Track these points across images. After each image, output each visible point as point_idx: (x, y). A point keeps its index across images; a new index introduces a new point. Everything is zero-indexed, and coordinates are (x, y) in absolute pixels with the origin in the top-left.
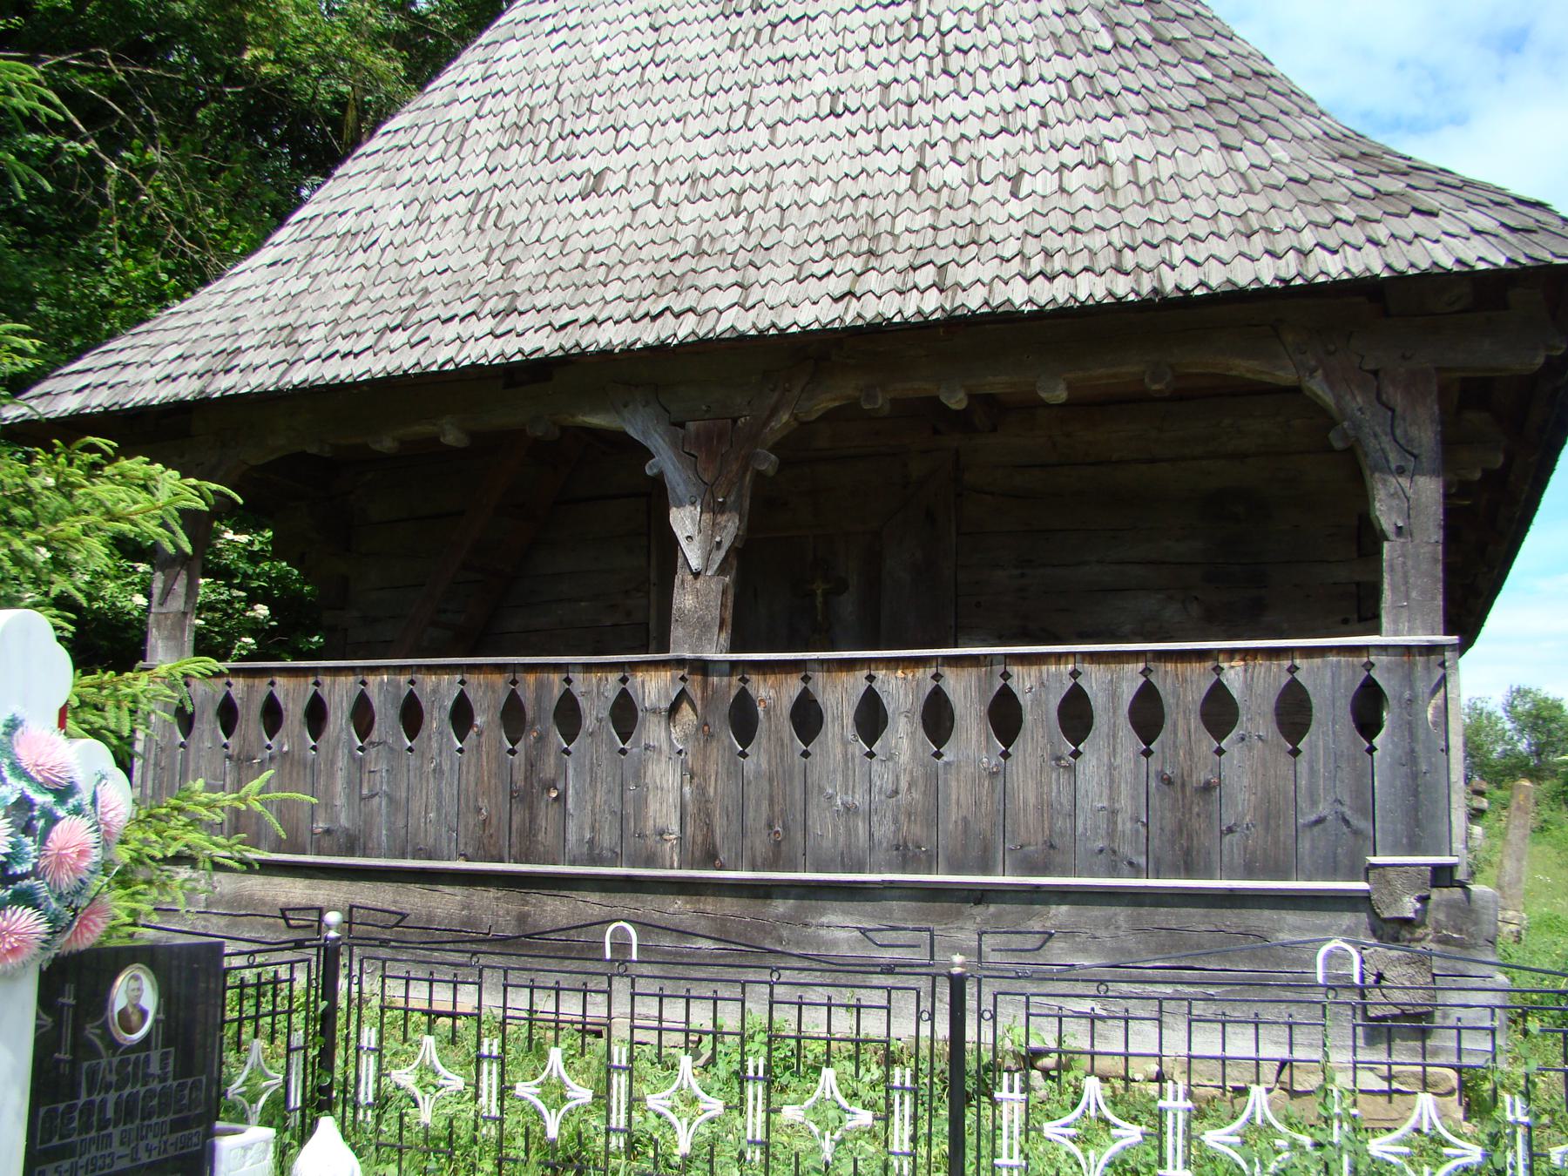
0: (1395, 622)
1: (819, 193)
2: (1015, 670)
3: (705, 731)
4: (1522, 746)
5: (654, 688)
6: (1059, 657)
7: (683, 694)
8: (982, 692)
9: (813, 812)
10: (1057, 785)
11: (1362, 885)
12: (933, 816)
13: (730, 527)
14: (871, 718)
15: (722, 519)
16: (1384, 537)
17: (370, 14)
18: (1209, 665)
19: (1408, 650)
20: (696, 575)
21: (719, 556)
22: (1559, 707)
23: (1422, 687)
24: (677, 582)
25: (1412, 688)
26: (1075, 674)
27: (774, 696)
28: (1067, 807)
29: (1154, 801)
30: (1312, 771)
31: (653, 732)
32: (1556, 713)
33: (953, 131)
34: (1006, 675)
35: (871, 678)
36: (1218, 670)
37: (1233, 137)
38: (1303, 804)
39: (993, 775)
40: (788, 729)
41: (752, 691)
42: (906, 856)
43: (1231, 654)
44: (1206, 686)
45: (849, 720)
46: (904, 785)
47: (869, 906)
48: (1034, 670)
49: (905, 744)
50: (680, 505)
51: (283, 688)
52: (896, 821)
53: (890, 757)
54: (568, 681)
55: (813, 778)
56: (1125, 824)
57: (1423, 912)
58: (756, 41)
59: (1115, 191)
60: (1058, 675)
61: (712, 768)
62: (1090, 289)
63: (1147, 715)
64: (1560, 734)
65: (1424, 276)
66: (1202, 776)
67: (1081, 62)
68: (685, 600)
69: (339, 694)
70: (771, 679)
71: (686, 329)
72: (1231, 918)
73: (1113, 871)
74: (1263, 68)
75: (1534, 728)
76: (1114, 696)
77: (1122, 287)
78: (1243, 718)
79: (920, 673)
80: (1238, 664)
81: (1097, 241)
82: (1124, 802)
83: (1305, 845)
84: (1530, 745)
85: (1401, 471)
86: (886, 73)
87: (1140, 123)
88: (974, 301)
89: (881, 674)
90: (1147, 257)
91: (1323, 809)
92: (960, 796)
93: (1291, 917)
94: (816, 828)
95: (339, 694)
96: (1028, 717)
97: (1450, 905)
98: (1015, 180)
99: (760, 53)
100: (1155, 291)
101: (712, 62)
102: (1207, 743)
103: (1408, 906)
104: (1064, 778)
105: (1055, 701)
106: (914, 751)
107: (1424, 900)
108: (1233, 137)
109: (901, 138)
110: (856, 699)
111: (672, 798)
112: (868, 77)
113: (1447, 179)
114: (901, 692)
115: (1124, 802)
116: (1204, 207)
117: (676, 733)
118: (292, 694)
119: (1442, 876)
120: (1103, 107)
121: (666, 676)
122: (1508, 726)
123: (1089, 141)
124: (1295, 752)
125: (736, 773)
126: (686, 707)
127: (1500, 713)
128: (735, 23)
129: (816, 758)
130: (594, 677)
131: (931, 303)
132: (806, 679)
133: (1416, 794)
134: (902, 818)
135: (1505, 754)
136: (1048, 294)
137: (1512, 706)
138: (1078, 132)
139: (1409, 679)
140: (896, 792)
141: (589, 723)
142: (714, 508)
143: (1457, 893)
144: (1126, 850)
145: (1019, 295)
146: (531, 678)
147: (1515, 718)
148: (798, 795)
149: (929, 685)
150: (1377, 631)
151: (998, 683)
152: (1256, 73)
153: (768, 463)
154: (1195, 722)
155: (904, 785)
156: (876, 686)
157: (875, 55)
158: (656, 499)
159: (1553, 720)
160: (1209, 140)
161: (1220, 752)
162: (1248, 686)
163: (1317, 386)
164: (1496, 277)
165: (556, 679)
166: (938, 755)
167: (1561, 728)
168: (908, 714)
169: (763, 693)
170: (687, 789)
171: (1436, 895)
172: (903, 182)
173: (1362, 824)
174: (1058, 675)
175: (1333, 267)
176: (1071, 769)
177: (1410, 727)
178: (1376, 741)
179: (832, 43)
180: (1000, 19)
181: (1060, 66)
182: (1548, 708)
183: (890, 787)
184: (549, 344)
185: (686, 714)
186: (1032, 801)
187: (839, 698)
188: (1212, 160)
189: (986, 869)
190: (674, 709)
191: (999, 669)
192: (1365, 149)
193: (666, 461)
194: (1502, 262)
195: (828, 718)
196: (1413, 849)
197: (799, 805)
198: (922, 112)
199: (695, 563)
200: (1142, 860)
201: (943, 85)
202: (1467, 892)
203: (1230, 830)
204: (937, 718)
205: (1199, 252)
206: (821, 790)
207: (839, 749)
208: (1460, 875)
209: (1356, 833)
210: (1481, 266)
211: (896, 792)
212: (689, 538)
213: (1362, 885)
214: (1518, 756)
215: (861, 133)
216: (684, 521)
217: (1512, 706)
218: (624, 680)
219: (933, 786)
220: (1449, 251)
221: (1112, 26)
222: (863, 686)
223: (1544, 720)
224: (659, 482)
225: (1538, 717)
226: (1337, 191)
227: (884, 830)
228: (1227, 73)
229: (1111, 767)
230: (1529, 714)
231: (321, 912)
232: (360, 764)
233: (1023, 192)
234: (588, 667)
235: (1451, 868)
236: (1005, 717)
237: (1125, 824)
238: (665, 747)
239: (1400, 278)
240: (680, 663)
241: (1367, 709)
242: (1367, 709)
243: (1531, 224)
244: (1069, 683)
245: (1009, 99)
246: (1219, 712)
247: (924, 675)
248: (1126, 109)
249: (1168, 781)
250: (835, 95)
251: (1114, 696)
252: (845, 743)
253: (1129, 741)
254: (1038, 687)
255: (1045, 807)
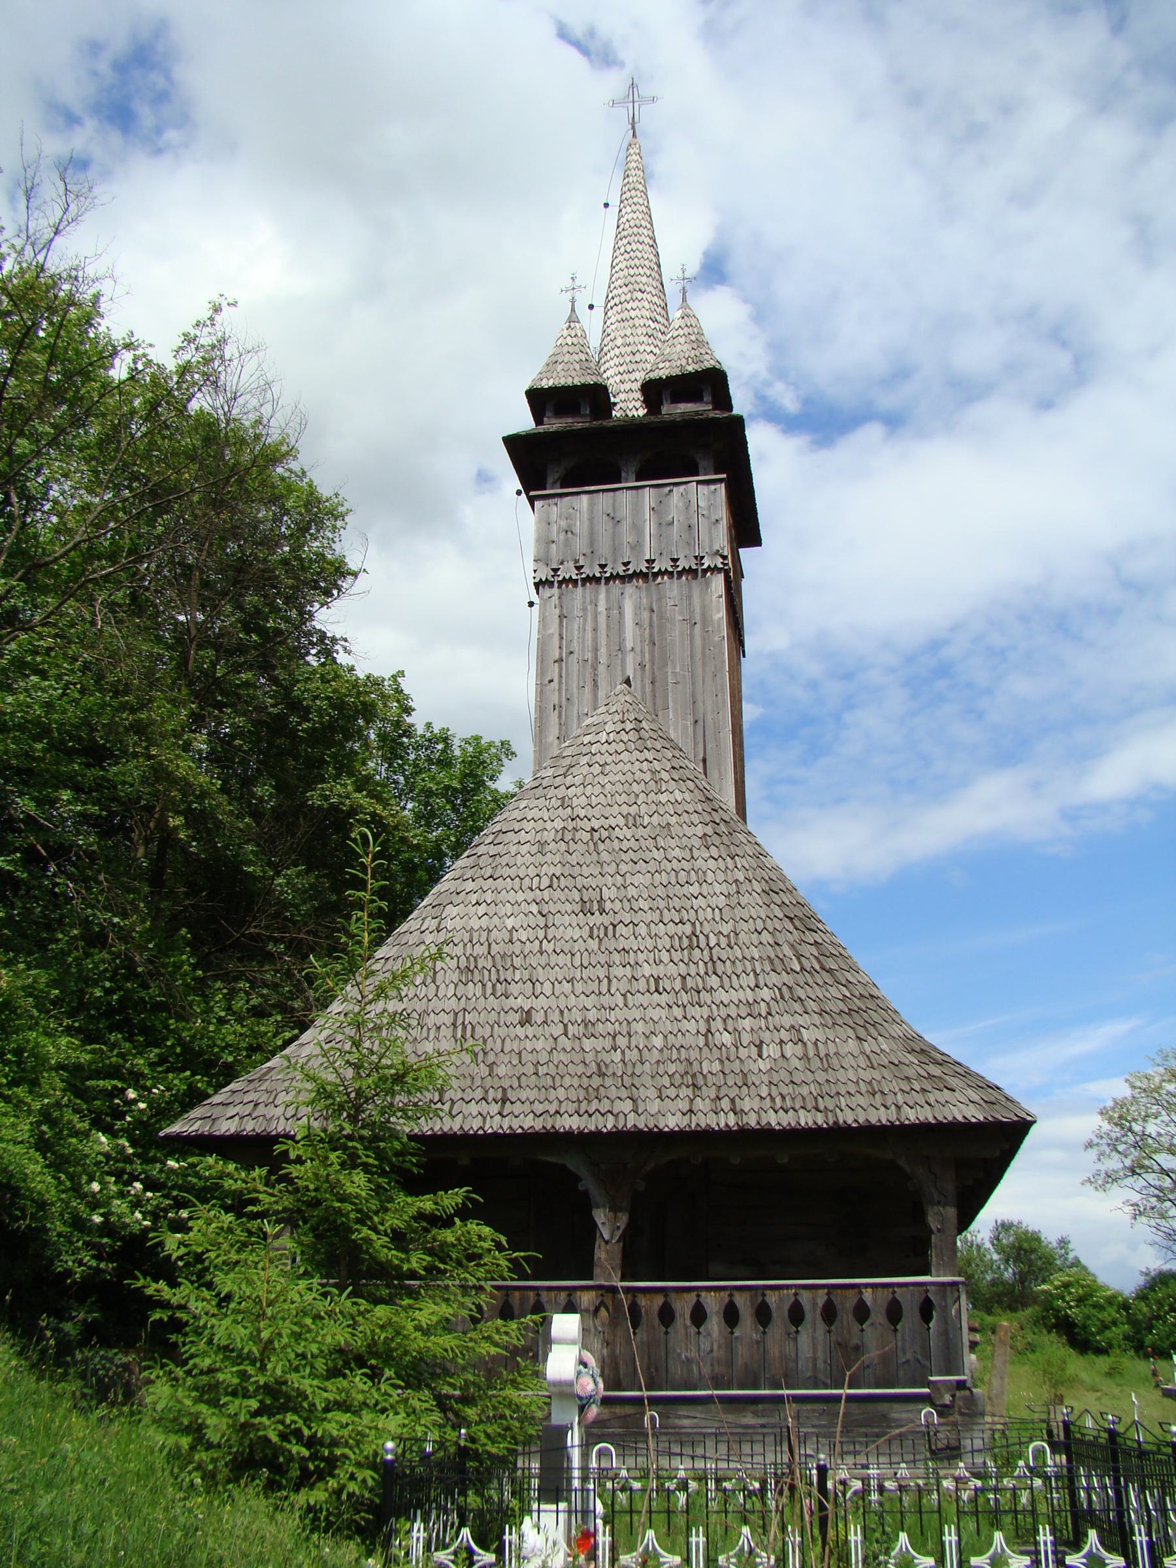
0: (938, 1271)
1: (658, 1041)
2: (768, 1292)
3: (614, 1322)
4: (1008, 1274)
6: (788, 1287)
7: (602, 1303)
8: (752, 1304)
9: (671, 1362)
10: (789, 1348)
11: (927, 1390)
12: (730, 1362)
13: (623, 1220)
14: (699, 1315)
15: (620, 1215)
16: (932, 1232)
18: (856, 1290)
19: (943, 1284)
20: (607, 1242)
21: (618, 1233)
22: (1038, 1240)
23: (949, 1301)
24: (597, 1246)
25: (946, 1301)
26: (796, 1294)
28: (793, 1355)
29: (834, 1354)
30: (903, 1339)
32: (1035, 1245)
33: (723, 1012)
34: (764, 1295)
35: (698, 1296)
36: (861, 1293)
37: (862, 1033)
38: (900, 1354)
39: (758, 1342)
40: (656, 1321)
41: (639, 1302)
42: (717, 1383)
43: (866, 1285)
44: (855, 1300)
45: (688, 1316)
46: (715, 1347)
47: (700, 1408)
48: (777, 1293)
49: (716, 1328)
50: (598, 1207)
52: (712, 1365)
53: (709, 1334)
54: (538, 1295)
55: (670, 1345)
56: (820, 1365)
57: (953, 1402)
58: (606, 935)
59: (809, 1059)
60: (788, 1295)
61: (618, 1340)
62: (806, 1119)
63: (829, 1313)
64: (1039, 1263)
65: (950, 1124)
66: (855, 1341)
67: (785, 978)
68: (600, 1254)
70: (648, 1296)
71: (609, 1124)
72: (870, 1407)
73: (816, 1387)
74: (875, 992)
75: (1017, 1259)
76: (815, 1304)
77: (820, 1119)
78: (872, 1315)
79: (722, 1293)
80: (869, 1290)
81: (805, 1090)
82: (820, 1354)
83: (901, 1373)
84: (1014, 1274)
85: (939, 1203)
86: (683, 969)
87: (817, 1019)
88: (752, 1121)
89: (703, 1294)
90: (829, 1103)
91: (909, 1356)
92: (743, 1353)
93: (897, 1406)
94: (672, 1369)
96: (774, 1315)
97: (964, 1398)
98: (759, 1047)
99: (610, 944)
100: (835, 1123)
101: (580, 945)
102: (856, 1327)
103: (947, 1399)
104: (792, 1343)
105: (786, 1307)
106: (720, 1331)
107: (953, 1396)
108: (862, 1033)
109: (696, 1011)
110: (691, 1306)
112: (672, 970)
113: (959, 1070)
114: (713, 1304)
115: (820, 1354)
116: (851, 1075)
117: (598, 1322)
119: (961, 1385)
120: (797, 1007)
122: (995, 1257)
123: (793, 1027)
124: (896, 1330)
126: (603, 1310)
127: (988, 1245)
128: (591, 920)
129: (672, 1336)
130: (553, 1294)
131: (732, 1120)
132: (666, 1296)
133: (948, 1348)
134: (715, 1363)
135: (993, 1283)
136: (786, 1120)
137: (997, 1238)
138: (787, 1020)
139: (944, 1298)
140: (712, 1351)
142: (615, 1209)
143: (967, 1393)
144: (822, 1377)
145: (774, 1120)
146: (517, 1294)
147: (1000, 1249)
148: (663, 1353)
149: (727, 1300)
150: (926, 1271)
151: (760, 1299)
152: (872, 996)
153: (641, 1186)
154: (851, 1316)
155: (715, 1347)
156: (701, 1300)
157: (677, 956)
158: (585, 1207)
159: (1033, 1251)
160: (851, 1033)
161: (862, 1330)
162: (874, 1300)
163: (902, 1163)
164: (979, 1125)
165: (532, 1294)
166: (732, 1333)
167: (1040, 1258)
168: (717, 1313)
169: (643, 1303)
170: (605, 1351)
171: (958, 1394)
172: (701, 1041)
173: (927, 1363)
174: (788, 1295)
175: (911, 1116)
176: (795, 1339)
177: (945, 1319)
178: (931, 1325)
179: (649, 943)
180: (740, 943)
181: (773, 978)
182: (1026, 1240)
183: (708, 1349)
184: (529, 1123)
185: (603, 1312)
186: (777, 1354)
187: (683, 1307)
188: (852, 1045)
189: (756, 1387)
190: (597, 1310)
191: (760, 1292)
192: (924, 1048)
193: (588, 1184)
194: (982, 1119)
195: (677, 1315)
196: (948, 1373)
197: (664, 1358)
198: (705, 997)
199: (606, 1236)
200: (829, 1382)
201: (714, 981)
202: (971, 1392)
203: (868, 1366)
204: (731, 1316)
205: (853, 1102)
206: (674, 1350)
207: (683, 1331)
208: (969, 1384)
209: (923, 1366)
210: (973, 1120)
211: (712, 1351)
212: (603, 1224)
213: (927, 1390)
214: (1003, 1283)
215: (675, 1007)
216: (600, 1216)
217: (997, 1238)
218: (570, 1295)
219: (730, 1346)
220: (960, 1111)
221: (799, 956)
222: (695, 1299)
223: (1026, 1251)
224: (586, 1194)
225: (1020, 1248)
226: (910, 1072)
227: (706, 1370)
228: (857, 994)
229: (813, 1338)
230: (1012, 1246)
233: (765, 1055)
234: (549, 1289)
235: (964, 1382)
236: (763, 1315)
237: (820, 1365)
238: (593, 1330)
239: (940, 1123)
240: (600, 1287)
241: (926, 1310)
242: (926, 1310)
243: (993, 1100)
244: (793, 1299)
245: (750, 996)
247: (725, 1295)
248: (810, 1011)
249: (840, 1344)
250: (657, 980)
251: (815, 1304)
252: (686, 1327)
253: (821, 1326)
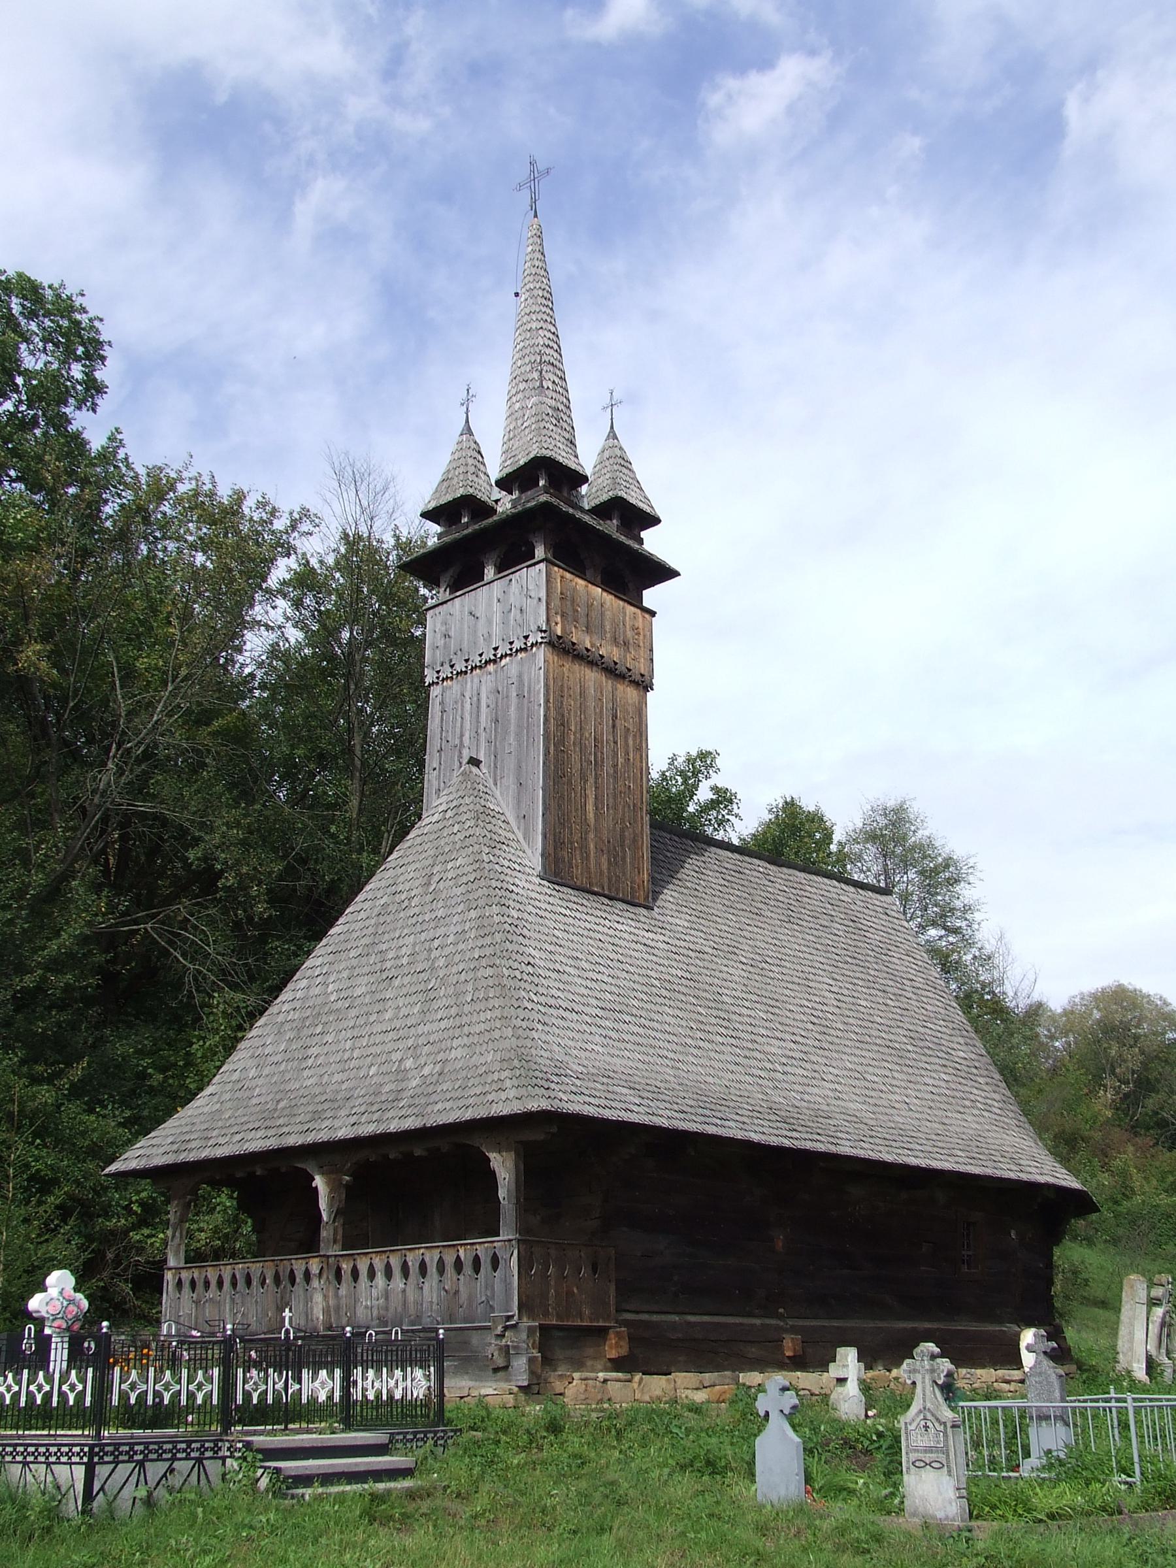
5: (315, 1266)
17: (1134, 1550)
27: (346, 1266)
31: (315, 1283)
51: (481, 1251)
69: (432, 1257)
95: (413, 1259)
111: (321, 1306)
118: (212, 1275)
121: (317, 1260)
125: (337, 1296)
141: (298, 1280)
216: (319, 1182)
231: (344, 1329)
232: (233, 1300)
246: (458, 1265)
247: (384, 1257)
251: (432, 1259)
254: (413, 1259)
255: (416, 1302)
